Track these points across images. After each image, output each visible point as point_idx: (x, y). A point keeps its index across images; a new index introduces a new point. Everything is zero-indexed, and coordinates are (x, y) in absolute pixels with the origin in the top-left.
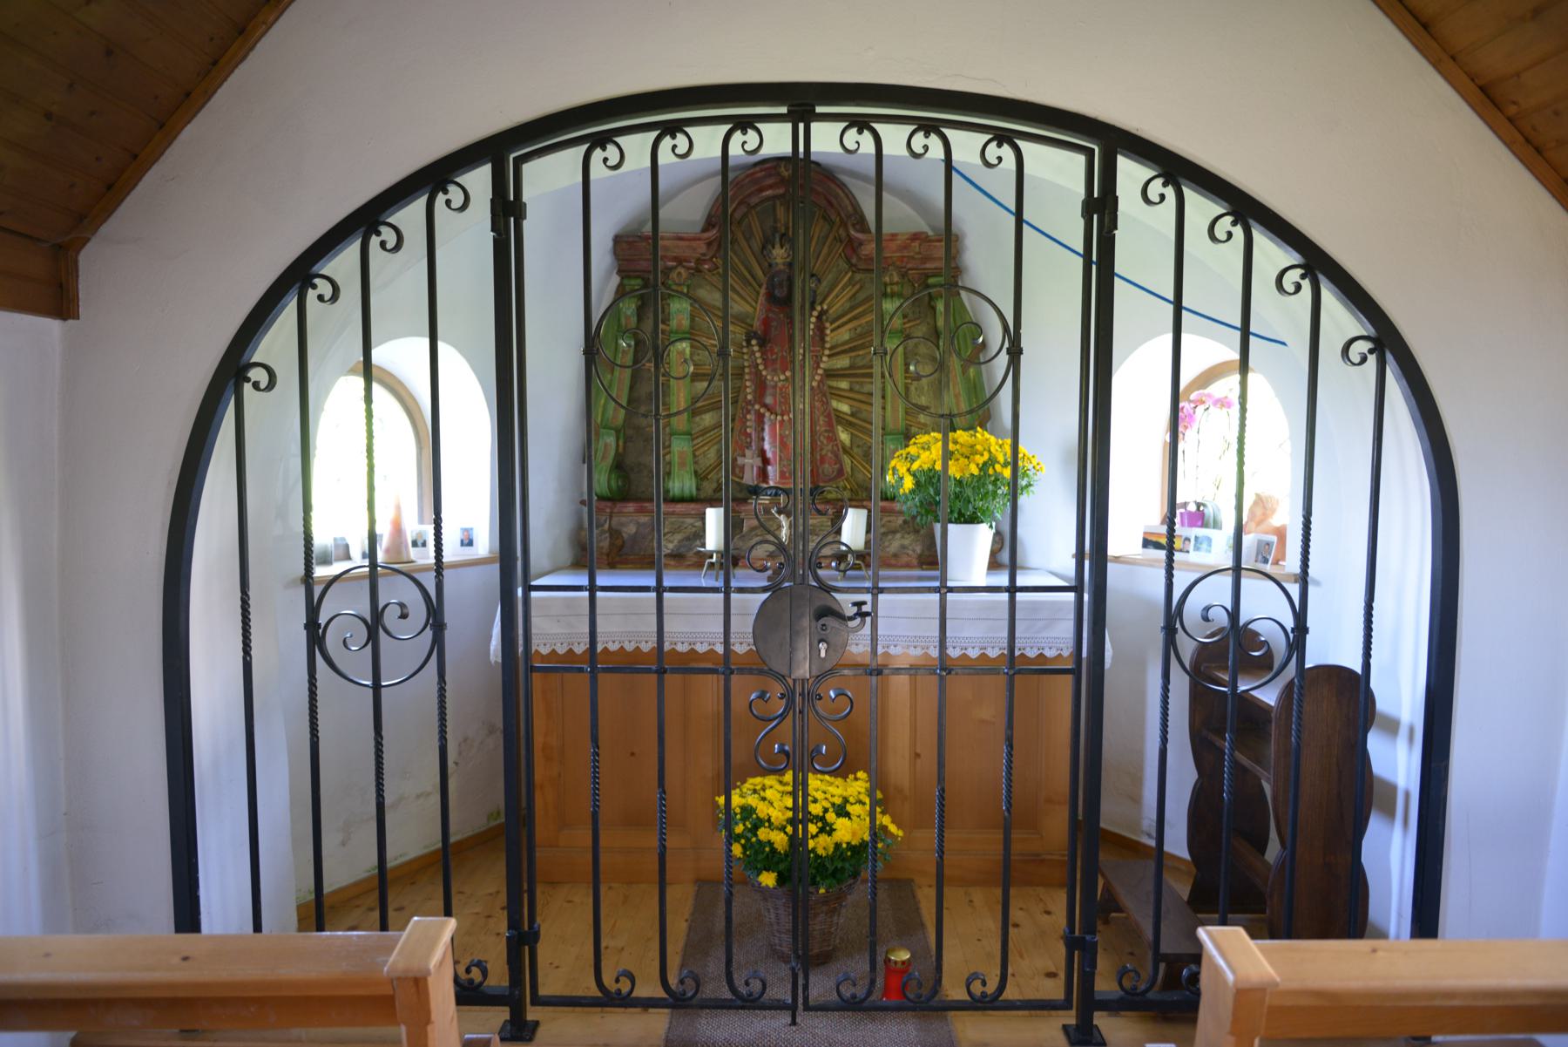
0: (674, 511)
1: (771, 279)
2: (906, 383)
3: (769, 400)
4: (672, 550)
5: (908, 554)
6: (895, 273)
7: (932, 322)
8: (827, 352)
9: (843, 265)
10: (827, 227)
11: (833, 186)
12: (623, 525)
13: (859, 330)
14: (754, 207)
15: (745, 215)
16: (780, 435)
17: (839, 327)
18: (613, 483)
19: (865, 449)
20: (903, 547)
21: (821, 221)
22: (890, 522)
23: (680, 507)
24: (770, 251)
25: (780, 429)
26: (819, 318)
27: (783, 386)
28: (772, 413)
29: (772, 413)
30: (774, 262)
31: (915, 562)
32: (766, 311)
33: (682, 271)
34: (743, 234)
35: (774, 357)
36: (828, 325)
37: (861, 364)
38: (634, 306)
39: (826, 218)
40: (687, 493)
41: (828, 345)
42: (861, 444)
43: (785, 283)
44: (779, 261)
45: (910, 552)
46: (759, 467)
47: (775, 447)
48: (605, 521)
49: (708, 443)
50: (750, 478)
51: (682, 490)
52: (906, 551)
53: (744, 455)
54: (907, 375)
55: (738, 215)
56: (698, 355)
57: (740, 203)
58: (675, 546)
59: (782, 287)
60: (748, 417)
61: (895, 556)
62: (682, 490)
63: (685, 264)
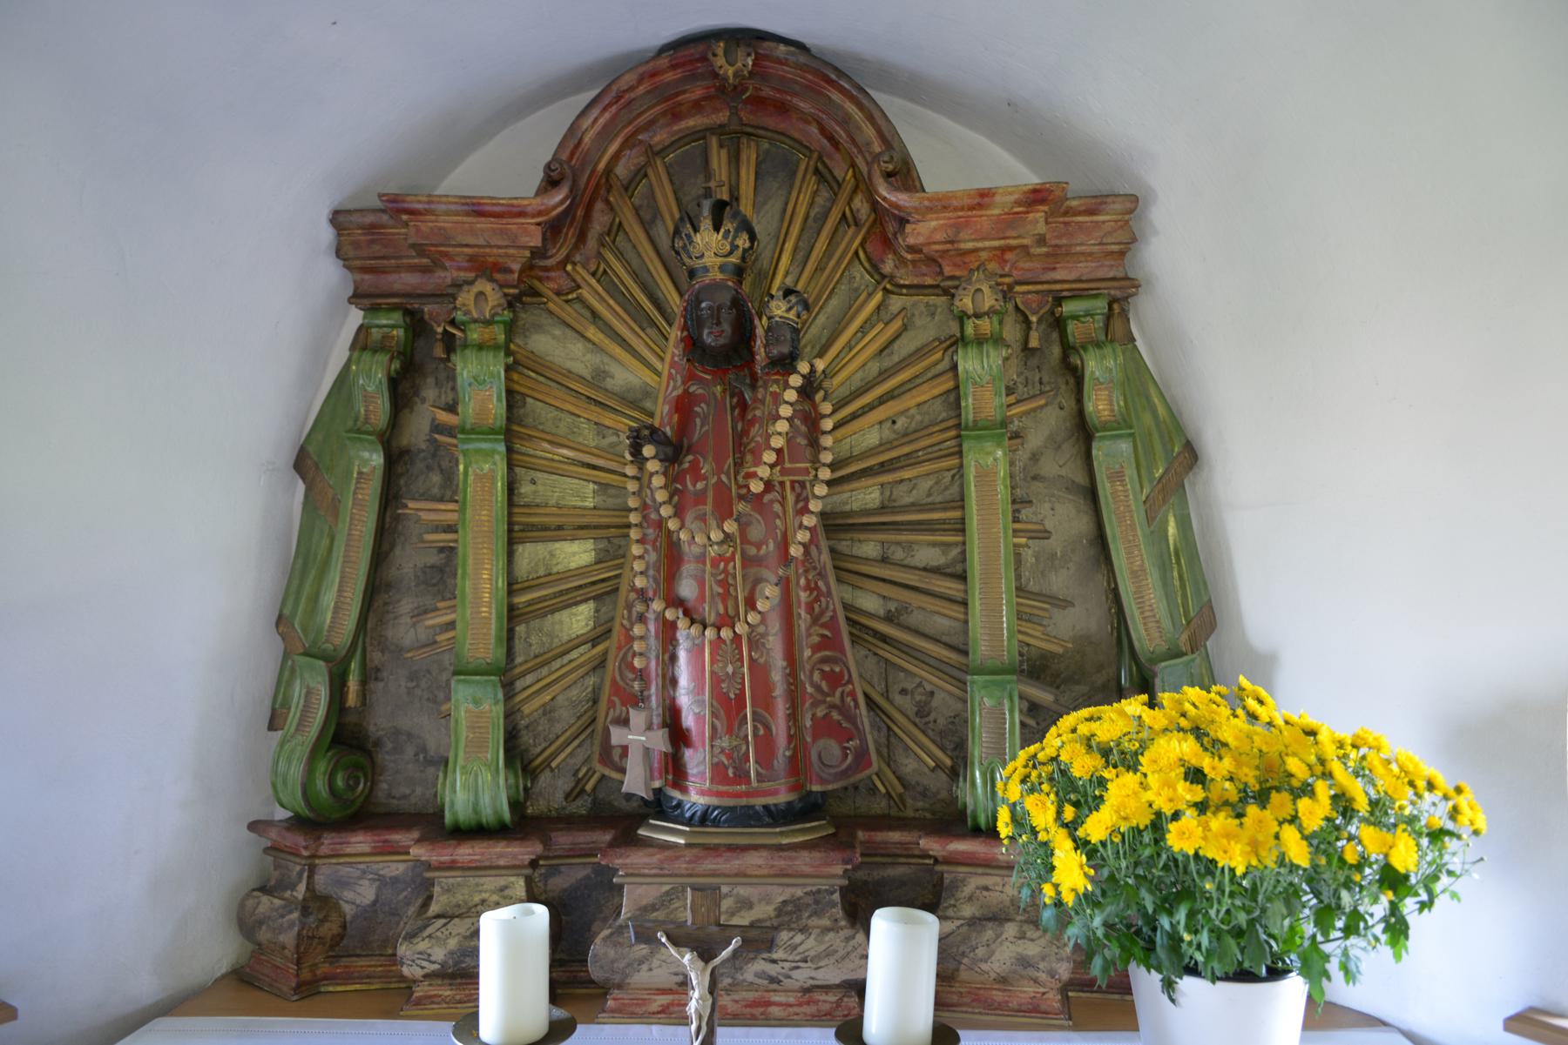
0: (454, 862)
1: (693, 307)
2: (1015, 545)
3: (687, 589)
4: (443, 965)
5: (1036, 981)
6: (985, 289)
7: (1069, 403)
8: (825, 474)
9: (860, 275)
10: (825, 193)
11: (836, 96)
12: (344, 884)
13: (901, 423)
14: (662, 152)
15: (640, 173)
16: (712, 673)
17: (854, 416)
18: (321, 784)
19: (918, 698)
20: (1024, 962)
21: (812, 181)
22: (986, 889)
23: (466, 852)
24: (688, 236)
25: (713, 662)
26: (807, 391)
27: (721, 558)
28: (693, 622)
29: (693, 622)
30: (698, 264)
31: (1054, 1000)
32: (684, 383)
33: (488, 288)
34: (637, 210)
35: (700, 485)
36: (826, 408)
37: (907, 500)
38: (380, 375)
39: (823, 175)
40: (487, 815)
41: (827, 457)
42: (909, 686)
43: (724, 313)
44: (710, 260)
45: (1043, 976)
46: (666, 754)
47: (701, 703)
48: (300, 874)
49: (549, 685)
50: (636, 781)
51: (476, 810)
52: (1031, 972)
53: (624, 722)
54: (1017, 526)
55: (621, 170)
56: (533, 482)
57: (628, 143)
58: (452, 953)
59: (718, 323)
60: (637, 630)
61: (1003, 980)
62: (476, 810)
63: (498, 276)
